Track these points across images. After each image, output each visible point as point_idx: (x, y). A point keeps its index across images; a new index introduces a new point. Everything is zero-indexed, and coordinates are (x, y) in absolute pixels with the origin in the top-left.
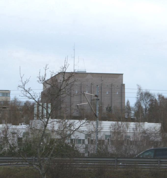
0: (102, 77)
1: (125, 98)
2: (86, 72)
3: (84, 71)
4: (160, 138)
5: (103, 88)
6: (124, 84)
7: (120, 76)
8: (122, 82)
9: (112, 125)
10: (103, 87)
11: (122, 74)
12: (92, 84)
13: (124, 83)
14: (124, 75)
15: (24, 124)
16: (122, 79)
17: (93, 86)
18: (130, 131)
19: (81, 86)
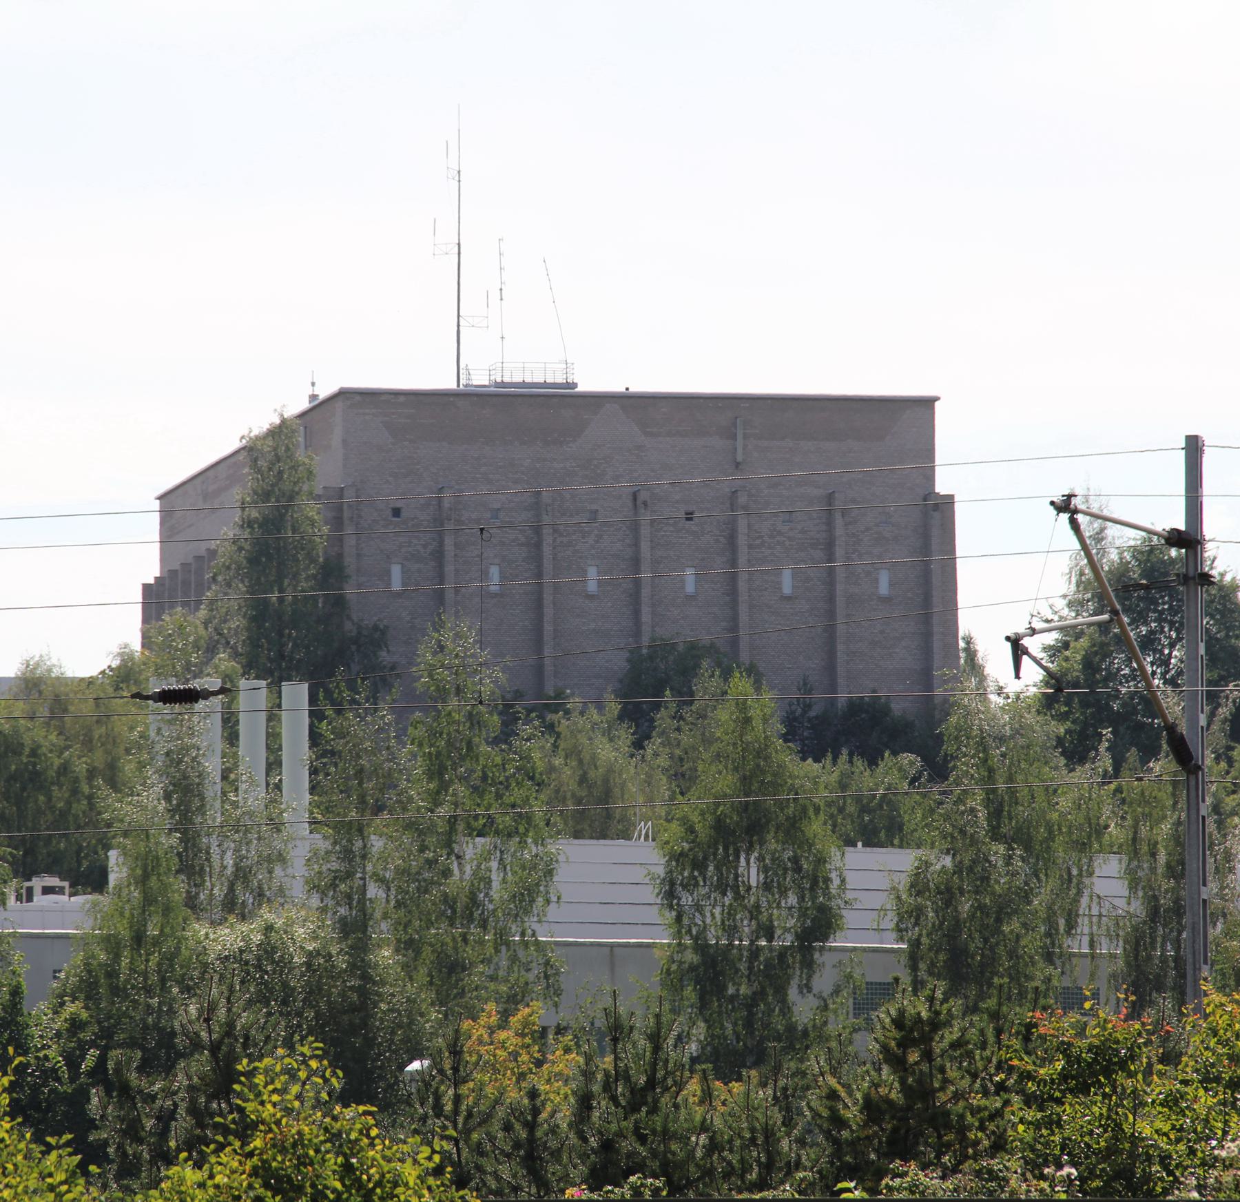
0: (734, 437)
1: (959, 611)
2: (575, 385)
3: (560, 379)
4: (527, 623)
5: (742, 540)
6: (951, 498)
7: (952, 497)
8: (929, 475)
9: (23, 744)
10: (742, 528)
11: (928, 404)
12: (643, 496)
13: (941, 487)
14: (942, 416)
15: (47, 890)
16: (934, 485)
17: (645, 517)
18: (1092, 945)
19: (537, 530)
